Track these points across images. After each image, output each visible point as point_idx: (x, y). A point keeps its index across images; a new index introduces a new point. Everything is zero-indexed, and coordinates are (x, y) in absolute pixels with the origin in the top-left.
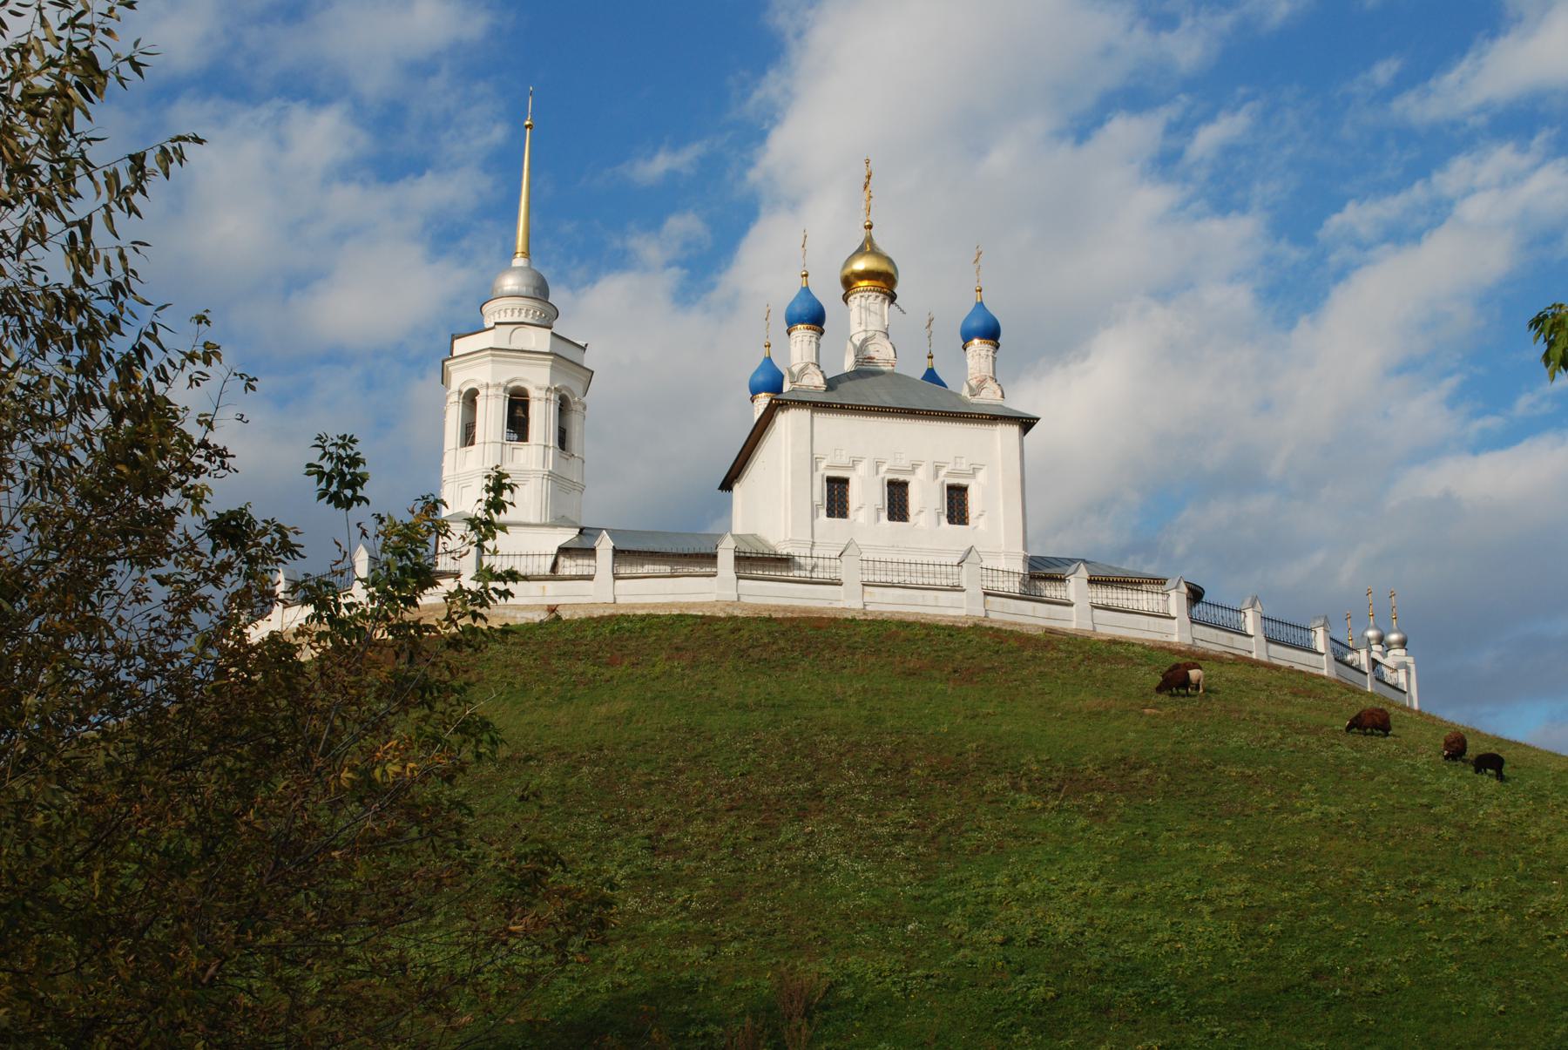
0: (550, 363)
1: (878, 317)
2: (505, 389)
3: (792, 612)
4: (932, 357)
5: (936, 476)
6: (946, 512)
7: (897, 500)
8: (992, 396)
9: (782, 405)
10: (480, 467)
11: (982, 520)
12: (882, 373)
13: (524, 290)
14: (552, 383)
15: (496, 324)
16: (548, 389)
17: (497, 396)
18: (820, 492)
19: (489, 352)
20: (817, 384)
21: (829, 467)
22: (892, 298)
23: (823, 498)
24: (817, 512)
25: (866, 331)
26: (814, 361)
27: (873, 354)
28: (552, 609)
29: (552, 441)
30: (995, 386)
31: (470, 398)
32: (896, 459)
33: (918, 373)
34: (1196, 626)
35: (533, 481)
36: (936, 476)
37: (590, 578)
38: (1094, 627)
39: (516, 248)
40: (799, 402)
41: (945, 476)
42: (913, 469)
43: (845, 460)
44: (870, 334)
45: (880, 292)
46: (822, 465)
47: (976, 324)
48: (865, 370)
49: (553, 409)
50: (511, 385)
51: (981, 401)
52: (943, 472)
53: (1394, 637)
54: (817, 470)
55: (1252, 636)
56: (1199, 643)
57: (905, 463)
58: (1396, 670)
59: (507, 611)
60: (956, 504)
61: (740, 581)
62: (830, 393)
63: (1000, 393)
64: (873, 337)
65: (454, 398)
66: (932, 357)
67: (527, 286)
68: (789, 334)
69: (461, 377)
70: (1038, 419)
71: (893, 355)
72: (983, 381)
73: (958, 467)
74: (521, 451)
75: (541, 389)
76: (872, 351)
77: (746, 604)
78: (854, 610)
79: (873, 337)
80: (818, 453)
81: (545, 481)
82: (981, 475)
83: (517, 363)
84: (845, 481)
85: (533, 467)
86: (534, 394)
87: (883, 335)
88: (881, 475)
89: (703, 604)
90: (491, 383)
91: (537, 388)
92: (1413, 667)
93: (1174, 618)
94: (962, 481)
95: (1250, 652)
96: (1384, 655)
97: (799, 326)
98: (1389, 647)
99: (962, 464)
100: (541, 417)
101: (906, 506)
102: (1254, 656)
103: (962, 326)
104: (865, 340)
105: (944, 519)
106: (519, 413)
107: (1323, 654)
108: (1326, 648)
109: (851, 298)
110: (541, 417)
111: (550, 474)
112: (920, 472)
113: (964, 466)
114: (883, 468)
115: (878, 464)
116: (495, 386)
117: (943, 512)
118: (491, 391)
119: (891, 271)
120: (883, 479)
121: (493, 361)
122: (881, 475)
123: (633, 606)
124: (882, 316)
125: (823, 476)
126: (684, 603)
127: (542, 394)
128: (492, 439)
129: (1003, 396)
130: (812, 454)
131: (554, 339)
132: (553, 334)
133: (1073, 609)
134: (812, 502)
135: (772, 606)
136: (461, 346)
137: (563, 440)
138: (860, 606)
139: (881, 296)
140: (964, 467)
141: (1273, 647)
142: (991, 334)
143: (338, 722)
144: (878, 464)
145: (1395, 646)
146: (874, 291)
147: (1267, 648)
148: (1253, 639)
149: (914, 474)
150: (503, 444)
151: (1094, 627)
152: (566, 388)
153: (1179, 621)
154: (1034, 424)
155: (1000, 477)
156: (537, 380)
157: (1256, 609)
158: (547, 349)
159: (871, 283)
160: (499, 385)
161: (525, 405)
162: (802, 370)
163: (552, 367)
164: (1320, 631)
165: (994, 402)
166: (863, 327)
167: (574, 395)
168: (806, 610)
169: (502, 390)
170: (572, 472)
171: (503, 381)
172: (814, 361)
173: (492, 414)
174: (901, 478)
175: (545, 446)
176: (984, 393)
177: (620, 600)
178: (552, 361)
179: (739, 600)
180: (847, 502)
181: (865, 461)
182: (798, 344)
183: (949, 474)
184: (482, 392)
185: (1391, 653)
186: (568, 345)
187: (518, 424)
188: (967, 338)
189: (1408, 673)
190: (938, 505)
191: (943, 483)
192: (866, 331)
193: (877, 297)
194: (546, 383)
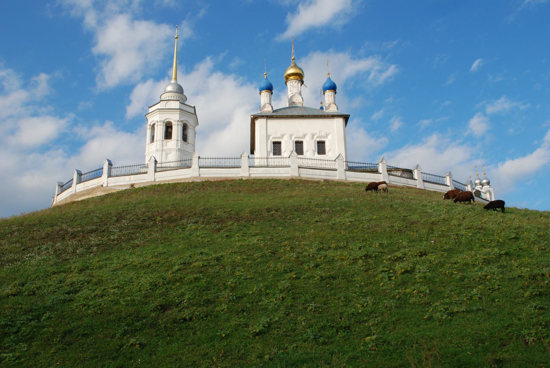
0: (179, 112)
1: (297, 89)
2: (164, 122)
3: (220, 179)
4: (322, 103)
5: (313, 138)
6: (317, 151)
7: (299, 147)
8: (333, 109)
9: (257, 117)
10: (176, 148)
11: (330, 152)
12: (298, 107)
13: (173, 90)
14: (180, 119)
15: (160, 101)
16: (178, 121)
17: (160, 125)
18: (270, 147)
19: (158, 110)
20: (270, 110)
21: (273, 138)
22: (302, 83)
23: (271, 149)
24: (269, 154)
25: (292, 93)
26: (269, 102)
27: (294, 101)
28: (132, 185)
29: (180, 138)
30: (334, 106)
31: (153, 127)
32: (297, 133)
33: (319, 108)
34: (390, 176)
35: (173, 152)
36: (313, 138)
37: (146, 173)
38: (346, 178)
39: (172, 77)
40: (261, 116)
41: (316, 138)
42: (304, 136)
43: (279, 135)
44: (294, 94)
45: (297, 80)
46: (271, 138)
47: (327, 85)
48: (292, 106)
49: (180, 128)
50: (166, 121)
51: (330, 111)
52: (315, 137)
53: (484, 181)
54: (269, 139)
55: (417, 180)
56: (393, 183)
57: (301, 134)
58: (485, 193)
59: (117, 187)
60: (321, 147)
61: (201, 169)
62: (274, 113)
63: (336, 108)
64: (295, 95)
65: (149, 127)
66: (322, 103)
67: (174, 89)
68: (260, 94)
69: (151, 120)
70: (349, 115)
71: (302, 100)
72: (330, 104)
73: (321, 134)
74: (169, 143)
75: (176, 121)
76: (294, 100)
77: (202, 177)
78: (245, 177)
79: (295, 95)
80: (269, 133)
81: (177, 152)
82: (329, 137)
83: (168, 113)
84: (280, 143)
85: (173, 148)
86: (174, 123)
87: (298, 94)
88: (293, 139)
89: (186, 179)
90: (158, 120)
91: (174, 121)
92: (492, 192)
93: (381, 173)
94: (323, 140)
95: (416, 186)
96: (481, 189)
97: (263, 91)
98: (482, 185)
99: (322, 133)
100: (176, 131)
101: (303, 150)
102: (418, 187)
103: (324, 84)
104: (292, 96)
105: (316, 153)
106: (170, 130)
107: (449, 186)
108: (450, 184)
109: (287, 83)
110: (176, 131)
111: (179, 149)
112: (307, 138)
113: (323, 134)
114: (293, 137)
115: (291, 136)
116: (160, 121)
117: (316, 151)
118: (159, 123)
119: (301, 72)
120: (293, 141)
121: (159, 113)
122: (293, 139)
123: (161, 181)
124: (298, 88)
125: (271, 141)
126: (179, 179)
127: (176, 123)
128: (159, 139)
129: (337, 109)
130: (267, 134)
131: (181, 104)
132: (180, 103)
133: (337, 172)
134: (267, 150)
135: (212, 177)
136: (151, 110)
137: (185, 138)
138: (248, 175)
139: (297, 81)
140: (323, 134)
141: (426, 184)
142: (333, 88)
143: (430, 281)
144: (291, 136)
145: (485, 185)
146: (294, 79)
147: (424, 184)
148: (417, 181)
149: (305, 138)
150: (163, 141)
151: (346, 178)
152: (185, 120)
153: (383, 175)
154: (349, 117)
155: (336, 136)
156: (174, 118)
157: (418, 169)
158: (178, 108)
159: (295, 77)
160: (161, 121)
161: (171, 127)
162: (264, 106)
163: (180, 114)
164: (448, 178)
165: (334, 111)
166: (291, 92)
167: (189, 123)
168: (218, 178)
169: (162, 122)
170: (188, 148)
171: (163, 119)
172: (269, 102)
173: (160, 131)
174: (300, 140)
175: (177, 140)
176: (330, 109)
177: (157, 180)
178: (180, 111)
179: (199, 176)
180: (281, 150)
181: (286, 135)
182: (263, 97)
183: (318, 137)
184: (156, 124)
185: (484, 187)
186: (189, 107)
187: (168, 135)
188: (325, 90)
189: (490, 194)
190: (313, 148)
191: (315, 140)
192: (292, 93)
193: (296, 81)
194: (178, 119)
